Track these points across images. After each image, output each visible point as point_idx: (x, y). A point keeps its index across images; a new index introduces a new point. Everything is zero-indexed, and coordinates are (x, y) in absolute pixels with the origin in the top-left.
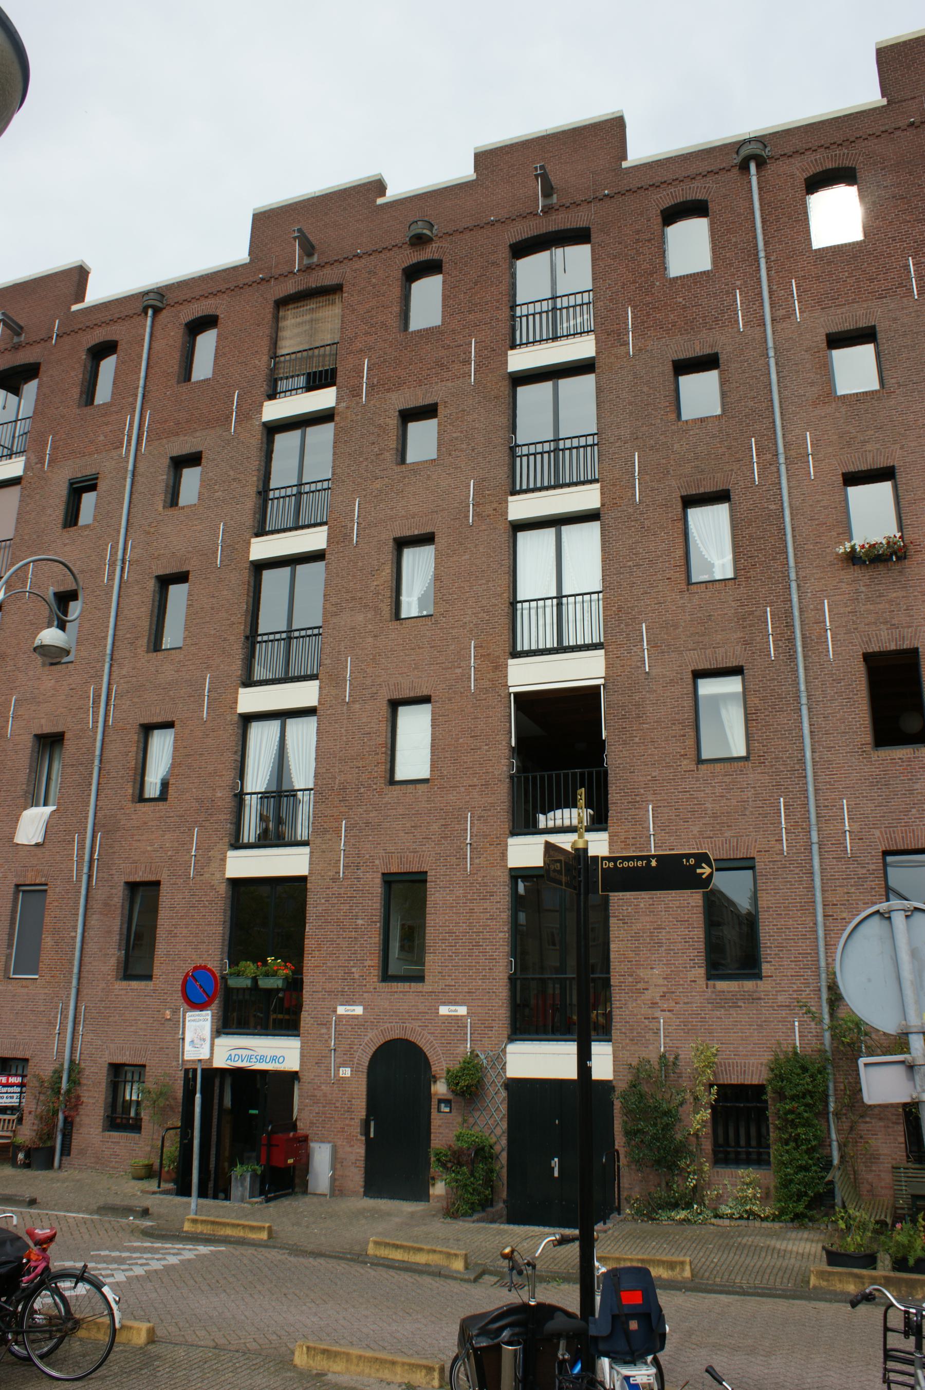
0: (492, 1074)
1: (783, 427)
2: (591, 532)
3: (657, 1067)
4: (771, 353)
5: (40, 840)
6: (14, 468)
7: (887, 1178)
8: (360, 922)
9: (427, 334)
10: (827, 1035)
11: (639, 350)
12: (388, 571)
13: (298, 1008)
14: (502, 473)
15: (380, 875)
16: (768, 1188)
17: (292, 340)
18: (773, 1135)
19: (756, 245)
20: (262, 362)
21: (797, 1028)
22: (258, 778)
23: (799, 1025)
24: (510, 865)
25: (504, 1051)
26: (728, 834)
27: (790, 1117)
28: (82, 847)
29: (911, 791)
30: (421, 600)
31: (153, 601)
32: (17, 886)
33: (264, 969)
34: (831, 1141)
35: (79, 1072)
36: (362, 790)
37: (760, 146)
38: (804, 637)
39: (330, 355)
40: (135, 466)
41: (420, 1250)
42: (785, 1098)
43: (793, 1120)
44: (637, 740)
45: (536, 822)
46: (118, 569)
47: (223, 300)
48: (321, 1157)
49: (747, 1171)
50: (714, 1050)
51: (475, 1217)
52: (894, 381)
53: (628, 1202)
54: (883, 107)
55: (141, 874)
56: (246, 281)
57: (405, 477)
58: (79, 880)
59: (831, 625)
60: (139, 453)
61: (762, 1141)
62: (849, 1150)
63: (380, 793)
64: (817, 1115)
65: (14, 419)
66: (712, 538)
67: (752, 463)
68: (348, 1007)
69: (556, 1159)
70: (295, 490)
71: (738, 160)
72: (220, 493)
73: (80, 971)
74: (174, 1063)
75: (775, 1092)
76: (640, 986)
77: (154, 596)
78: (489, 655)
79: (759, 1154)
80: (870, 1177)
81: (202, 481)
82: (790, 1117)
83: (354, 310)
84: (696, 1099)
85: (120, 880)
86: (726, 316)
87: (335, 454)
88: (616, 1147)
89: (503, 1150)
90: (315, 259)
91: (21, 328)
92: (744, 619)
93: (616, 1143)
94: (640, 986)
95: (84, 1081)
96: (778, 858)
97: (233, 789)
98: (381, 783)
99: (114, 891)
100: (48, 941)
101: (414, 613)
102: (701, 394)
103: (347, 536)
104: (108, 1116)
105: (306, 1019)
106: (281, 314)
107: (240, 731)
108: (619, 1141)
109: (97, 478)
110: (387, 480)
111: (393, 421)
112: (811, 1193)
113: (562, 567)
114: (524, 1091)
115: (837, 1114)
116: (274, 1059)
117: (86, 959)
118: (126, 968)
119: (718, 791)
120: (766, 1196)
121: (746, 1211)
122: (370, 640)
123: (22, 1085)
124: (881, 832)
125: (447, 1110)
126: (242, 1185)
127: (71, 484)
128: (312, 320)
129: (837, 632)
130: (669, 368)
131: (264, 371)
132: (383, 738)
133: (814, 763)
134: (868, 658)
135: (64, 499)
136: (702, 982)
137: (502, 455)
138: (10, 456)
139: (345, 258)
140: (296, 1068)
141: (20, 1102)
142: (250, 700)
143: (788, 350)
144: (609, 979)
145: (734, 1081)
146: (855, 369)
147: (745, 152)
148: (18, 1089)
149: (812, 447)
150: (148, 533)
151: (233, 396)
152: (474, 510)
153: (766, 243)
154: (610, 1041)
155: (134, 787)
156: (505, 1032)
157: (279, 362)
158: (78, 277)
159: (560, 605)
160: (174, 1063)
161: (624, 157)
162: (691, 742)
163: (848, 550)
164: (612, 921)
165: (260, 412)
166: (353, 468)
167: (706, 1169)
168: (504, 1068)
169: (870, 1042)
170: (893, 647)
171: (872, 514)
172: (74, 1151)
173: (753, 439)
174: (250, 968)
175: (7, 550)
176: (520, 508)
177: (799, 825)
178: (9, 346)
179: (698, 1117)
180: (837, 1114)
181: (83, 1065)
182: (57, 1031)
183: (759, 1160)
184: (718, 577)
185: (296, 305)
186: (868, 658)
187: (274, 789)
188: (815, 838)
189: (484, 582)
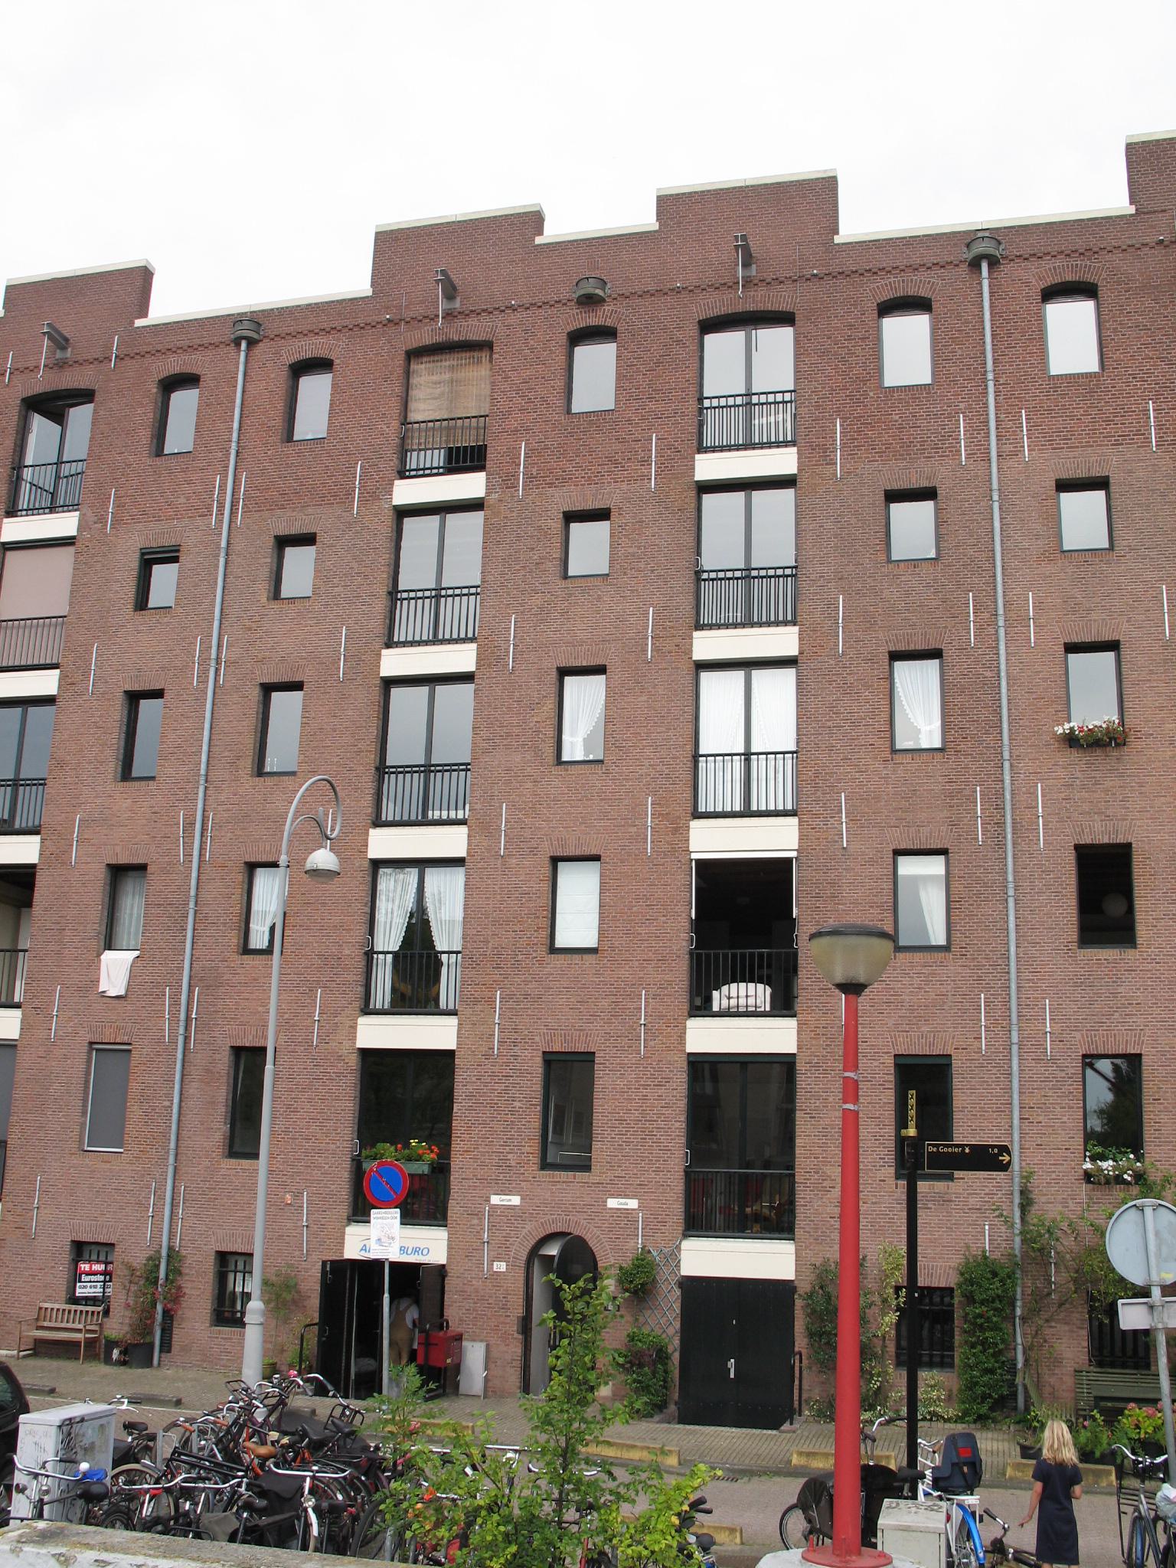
2: (787, 678)
7: (1069, 1381)
8: (517, 1104)
10: (1018, 1239)
12: (550, 704)
14: (686, 602)
15: (540, 1054)
16: (950, 1390)
18: (958, 1338)
22: (390, 937)
25: (678, 1248)
26: (925, 1029)
28: (175, 1002)
29: (1115, 994)
30: (587, 742)
32: (91, 1043)
39: (477, 428)
40: (228, 543)
41: (633, 1447)
42: (974, 1302)
45: (708, 1000)
47: (339, 340)
48: (474, 1355)
51: (657, 1418)
52: (1125, 543)
54: (1131, 215)
58: (173, 1041)
62: (1032, 1354)
63: (541, 962)
64: (1004, 1319)
66: (919, 705)
71: (970, 256)
73: (177, 1147)
75: (964, 1295)
79: (942, 1356)
80: (1052, 1380)
83: (507, 377)
84: (885, 1301)
86: (946, 445)
88: (797, 1349)
91: (67, 340)
92: (952, 798)
95: (185, 1271)
98: (542, 951)
99: (217, 1056)
100: (135, 1112)
101: (579, 757)
102: (913, 527)
103: (501, 659)
105: (454, 1208)
106: (412, 366)
108: (801, 1342)
109: (178, 551)
111: (557, 524)
113: (750, 716)
114: (702, 1294)
115: (1023, 1319)
116: (416, 1250)
118: (231, 1146)
119: (916, 981)
120: (949, 1398)
122: (529, 785)
123: (105, 1273)
134: (1077, 847)
135: (135, 573)
140: (443, 1261)
142: (383, 843)
144: (793, 1175)
146: (1083, 518)
147: (980, 248)
148: (102, 1278)
150: (250, 629)
151: (355, 467)
156: (681, 1229)
158: (140, 280)
159: (748, 761)
164: (798, 1114)
165: (390, 493)
168: (678, 1266)
169: (1060, 1248)
171: (1093, 697)
174: (388, 1150)
176: (707, 645)
177: (1000, 1024)
179: (887, 1319)
180: (1023, 1319)
181: (184, 1252)
186: (1077, 847)
188: (1015, 1039)
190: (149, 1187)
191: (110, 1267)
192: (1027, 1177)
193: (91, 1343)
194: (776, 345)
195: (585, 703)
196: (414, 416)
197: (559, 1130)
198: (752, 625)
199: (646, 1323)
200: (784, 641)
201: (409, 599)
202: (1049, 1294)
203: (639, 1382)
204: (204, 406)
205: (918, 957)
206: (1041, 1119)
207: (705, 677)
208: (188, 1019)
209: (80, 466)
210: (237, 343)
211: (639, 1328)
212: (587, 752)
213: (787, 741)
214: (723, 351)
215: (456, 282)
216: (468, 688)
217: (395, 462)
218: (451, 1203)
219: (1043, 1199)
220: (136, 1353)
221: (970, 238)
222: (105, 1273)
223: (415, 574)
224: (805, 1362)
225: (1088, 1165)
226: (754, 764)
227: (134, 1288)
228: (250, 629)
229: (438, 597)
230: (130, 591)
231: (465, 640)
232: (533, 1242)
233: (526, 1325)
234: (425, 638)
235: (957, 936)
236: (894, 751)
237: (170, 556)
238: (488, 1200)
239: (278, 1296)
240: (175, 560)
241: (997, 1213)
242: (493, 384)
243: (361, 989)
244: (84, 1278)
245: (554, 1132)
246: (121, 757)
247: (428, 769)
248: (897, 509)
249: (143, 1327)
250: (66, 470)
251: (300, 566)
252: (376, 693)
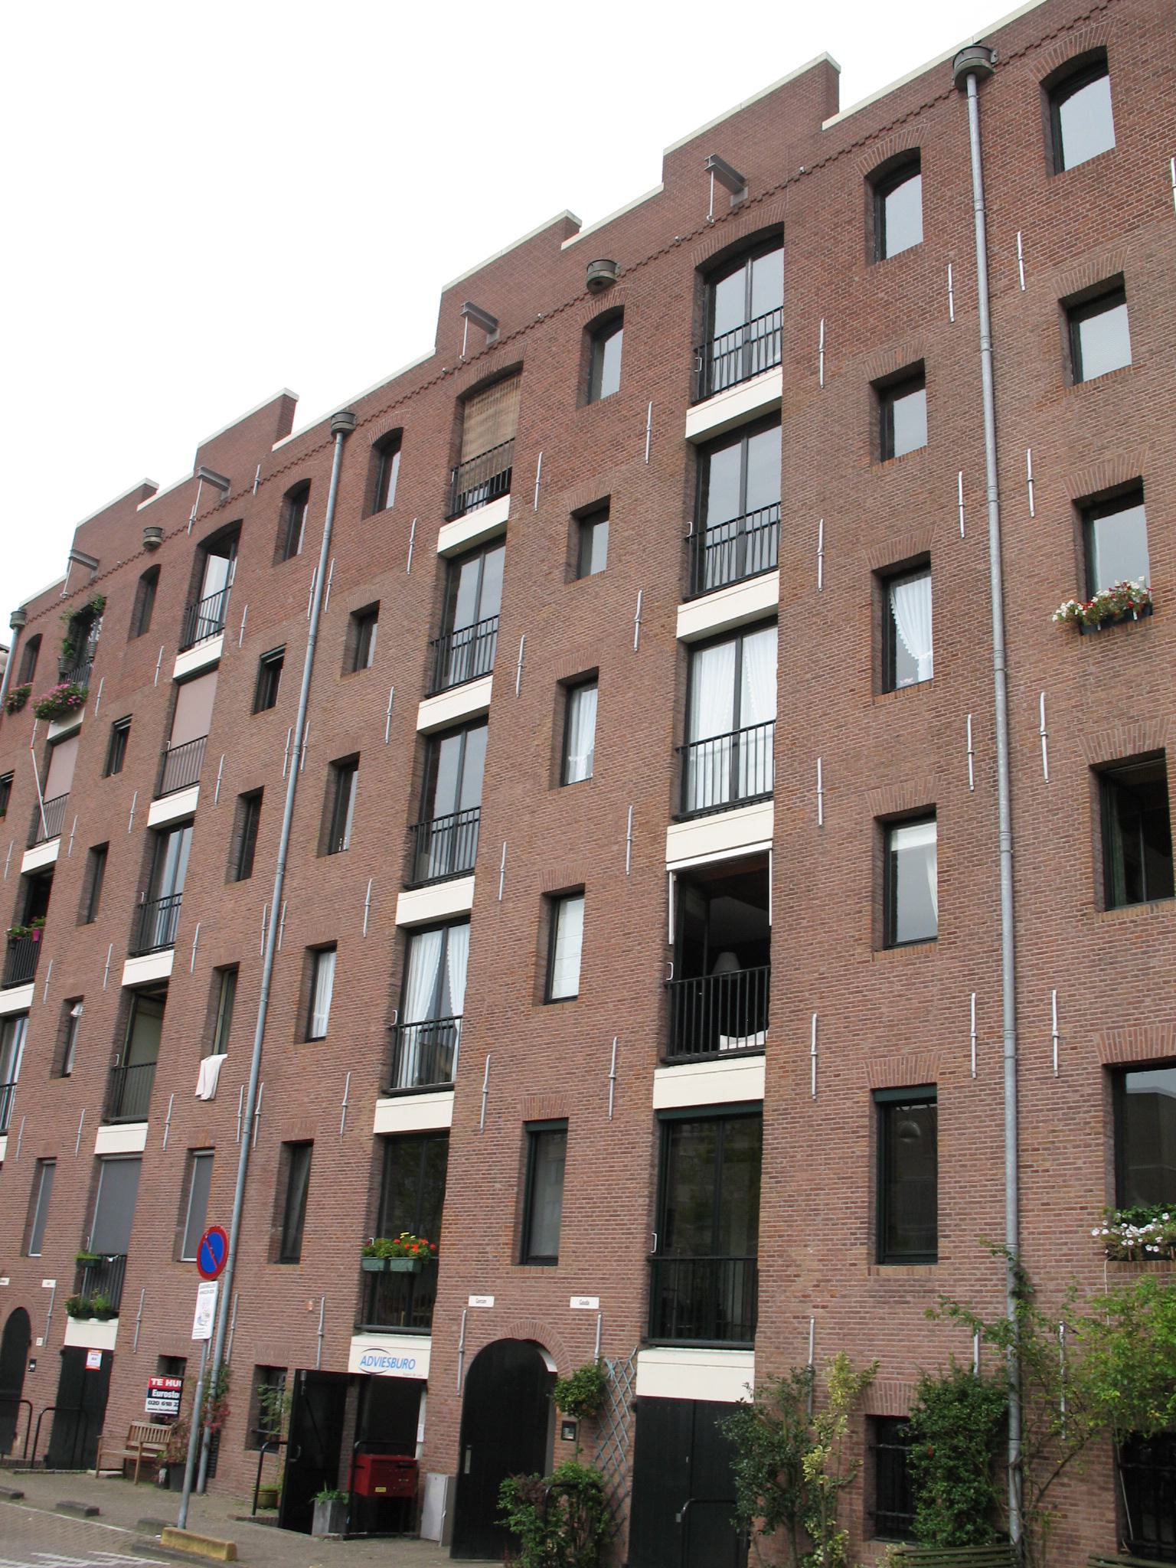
0: (619, 1391)
8: (498, 1186)
11: (831, 376)
13: (429, 1300)
15: (520, 1124)
24: (658, 1104)
25: (635, 1358)
31: (327, 793)
44: (804, 923)
45: (716, 1044)
46: (294, 757)
76: (791, 1271)
77: (328, 787)
85: (279, 1139)
89: (627, 1495)
90: (497, 336)
91: (495, 321)
94: (791, 1271)
95: (232, 1387)
97: (389, 1020)
104: (254, 1432)
106: (467, 412)
107: (400, 948)
113: (739, 694)
114: (661, 1417)
116: (405, 1363)
117: (243, 1238)
119: (897, 988)
122: (527, 817)
123: (179, 1390)
124: (1102, 1036)
126: (324, 1516)
127: (263, 660)
136: (863, 1266)
140: (425, 1377)
142: (413, 907)
147: (959, 66)
148: (177, 1395)
155: (297, 1026)
159: (736, 745)
164: (764, 1179)
168: (633, 1383)
172: (219, 1472)
178: (216, 505)
181: (233, 1367)
187: (432, 1018)
206: (1047, 1165)
222: (179, 1390)
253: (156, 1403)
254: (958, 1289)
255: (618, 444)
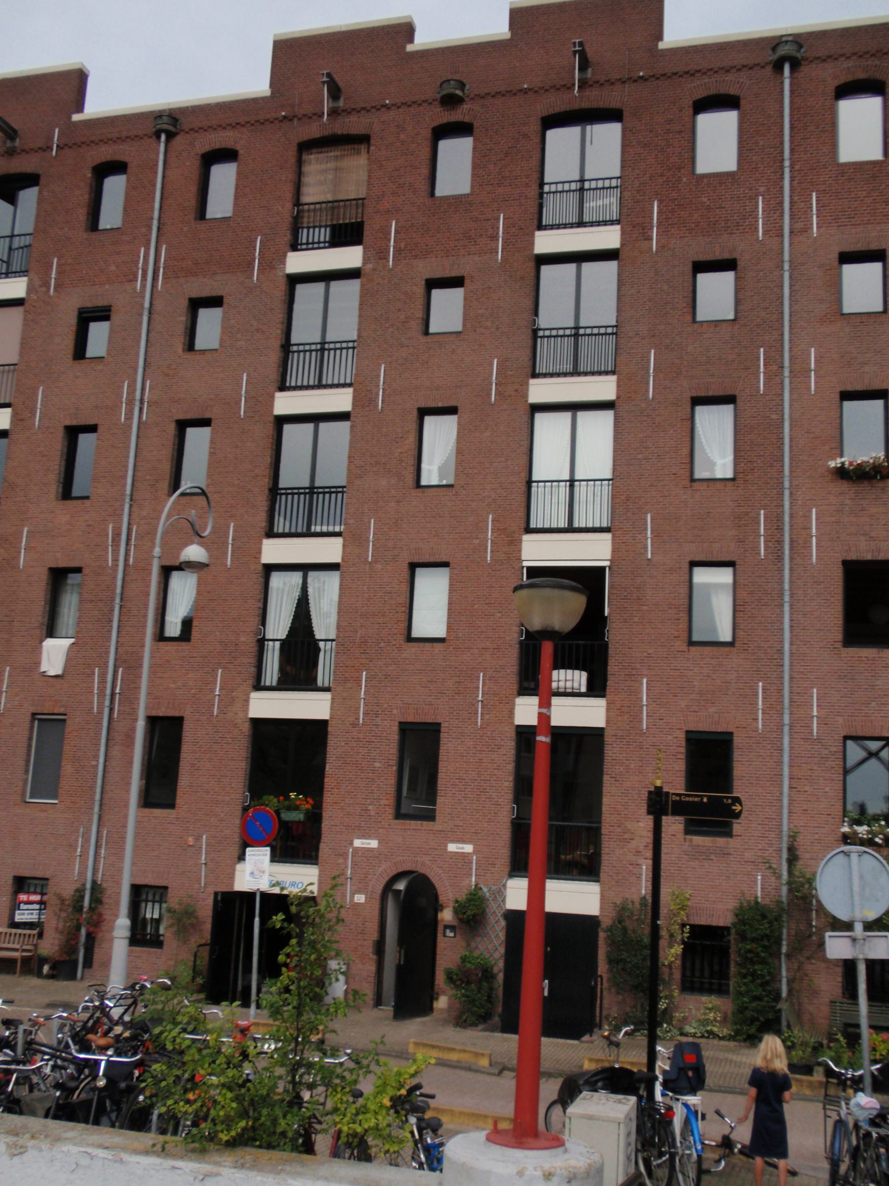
0: (492, 907)
1: (791, 340)
2: (606, 418)
3: (638, 906)
4: (786, 266)
5: (60, 672)
6: (16, 288)
7: (826, 1010)
8: (377, 765)
9: (456, 201)
12: (412, 439)
15: (397, 724)
16: (726, 1014)
17: (316, 189)
18: (733, 969)
19: (782, 152)
20: (286, 209)
21: (759, 882)
22: (279, 625)
23: (762, 879)
25: (505, 886)
26: (712, 710)
27: (750, 955)
28: (103, 681)
30: (441, 469)
32: (34, 714)
33: (287, 803)
34: (782, 977)
35: (101, 892)
36: (382, 645)
37: (795, 47)
38: (792, 541)
40: (151, 304)
43: (752, 959)
44: (636, 619)
49: (709, 999)
50: (687, 896)
51: (481, 1027)
53: (608, 1020)
55: (163, 709)
56: (268, 116)
57: (430, 349)
58: (101, 712)
59: (817, 532)
60: (155, 289)
61: (724, 975)
63: (399, 649)
65: (8, 233)
67: (758, 372)
68: (364, 841)
69: (547, 981)
70: (319, 347)
71: (774, 57)
72: (242, 343)
74: (196, 886)
75: (738, 933)
76: (626, 836)
78: (505, 529)
81: (224, 329)
82: (750, 955)
84: (672, 936)
87: (360, 316)
88: (599, 973)
89: (500, 971)
91: (15, 131)
93: (599, 969)
94: (626, 836)
95: (105, 900)
96: (754, 734)
98: (401, 639)
100: (68, 768)
101: (435, 481)
102: (716, 294)
103: (373, 401)
105: (324, 849)
107: (263, 580)
108: (602, 967)
109: (110, 310)
110: (412, 349)
112: (762, 1019)
113: (575, 447)
117: (107, 788)
120: (725, 1020)
121: (707, 1031)
122: (393, 504)
123: (41, 903)
125: (452, 935)
128: (336, 169)
129: (823, 537)
130: (689, 268)
131: (287, 220)
132: (404, 598)
133: (792, 654)
134: (846, 564)
135: (74, 328)
136: (681, 836)
137: (525, 337)
138: (7, 275)
139: (373, 107)
141: (39, 918)
142: (274, 551)
143: (802, 264)
145: (703, 923)
146: (863, 287)
147: (783, 50)
148: (37, 906)
149: (815, 363)
150: (168, 375)
152: (496, 389)
153: (792, 151)
154: (598, 881)
156: (507, 870)
157: (303, 211)
158: (77, 80)
159: (572, 486)
160: (196, 886)
161: (660, 37)
162: (684, 626)
163: (839, 465)
165: (284, 263)
166: (379, 333)
167: (676, 994)
168: (504, 901)
170: (869, 557)
173: (762, 350)
174: (272, 801)
175: (11, 374)
176: (540, 391)
177: (774, 707)
179: (673, 951)
180: (788, 956)
181: (105, 885)
182: (78, 854)
183: (721, 990)
184: (719, 475)
185: (320, 150)
186: (846, 564)
188: (786, 719)
189: (503, 459)
190: (77, 831)
191: (45, 898)
192: (793, 837)
193: (26, 961)
194: (607, 138)
195: (440, 439)
196: (305, 199)
197: (412, 787)
198: (579, 374)
199: (477, 948)
200: (604, 388)
201: (299, 352)
202: (810, 936)
203: (467, 996)
204: (130, 189)
205: (707, 650)
206: (807, 788)
207: (539, 417)
208: (113, 694)
209: (27, 240)
210: (157, 135)
211: (471, 952)
212: (441, 477)
213: (606, 472)
214: (561, 143)
215: (340, 84)
216: (345, 426)
217: (288, 237)
218: (322, 846)
219: (807, 856)
220: (64, 968)
221: (775, 42)
222: (41, 903)
223: (305, 331)
224: (605, 984)
225: (846, 829)
226: (576, 489)
227: (63, 915)
228: (168, 375)
229: (323, 350)
230: (68, 342)
231: (344, 385)
232: (387, 879)
233: (379, 947)
234: (311, 383)
235: (741, 634)
236: (693, 480)
237: (103, 314)
238: (351, 844)
239: (179, 920)
240: (107, 318)
241: (767, 865)
242: (370, 171)
243: (253, 670)
244: (22, 906)
245: (409, 789)
246: (62, 480)
247: (312, 490)
248: (848, 270)
249: (70, 948)
250: (16, 243)
251: (210, 323)
252: (270, 429)
253: (23, 914)
254: (746, 854)
255: (469, 238)
